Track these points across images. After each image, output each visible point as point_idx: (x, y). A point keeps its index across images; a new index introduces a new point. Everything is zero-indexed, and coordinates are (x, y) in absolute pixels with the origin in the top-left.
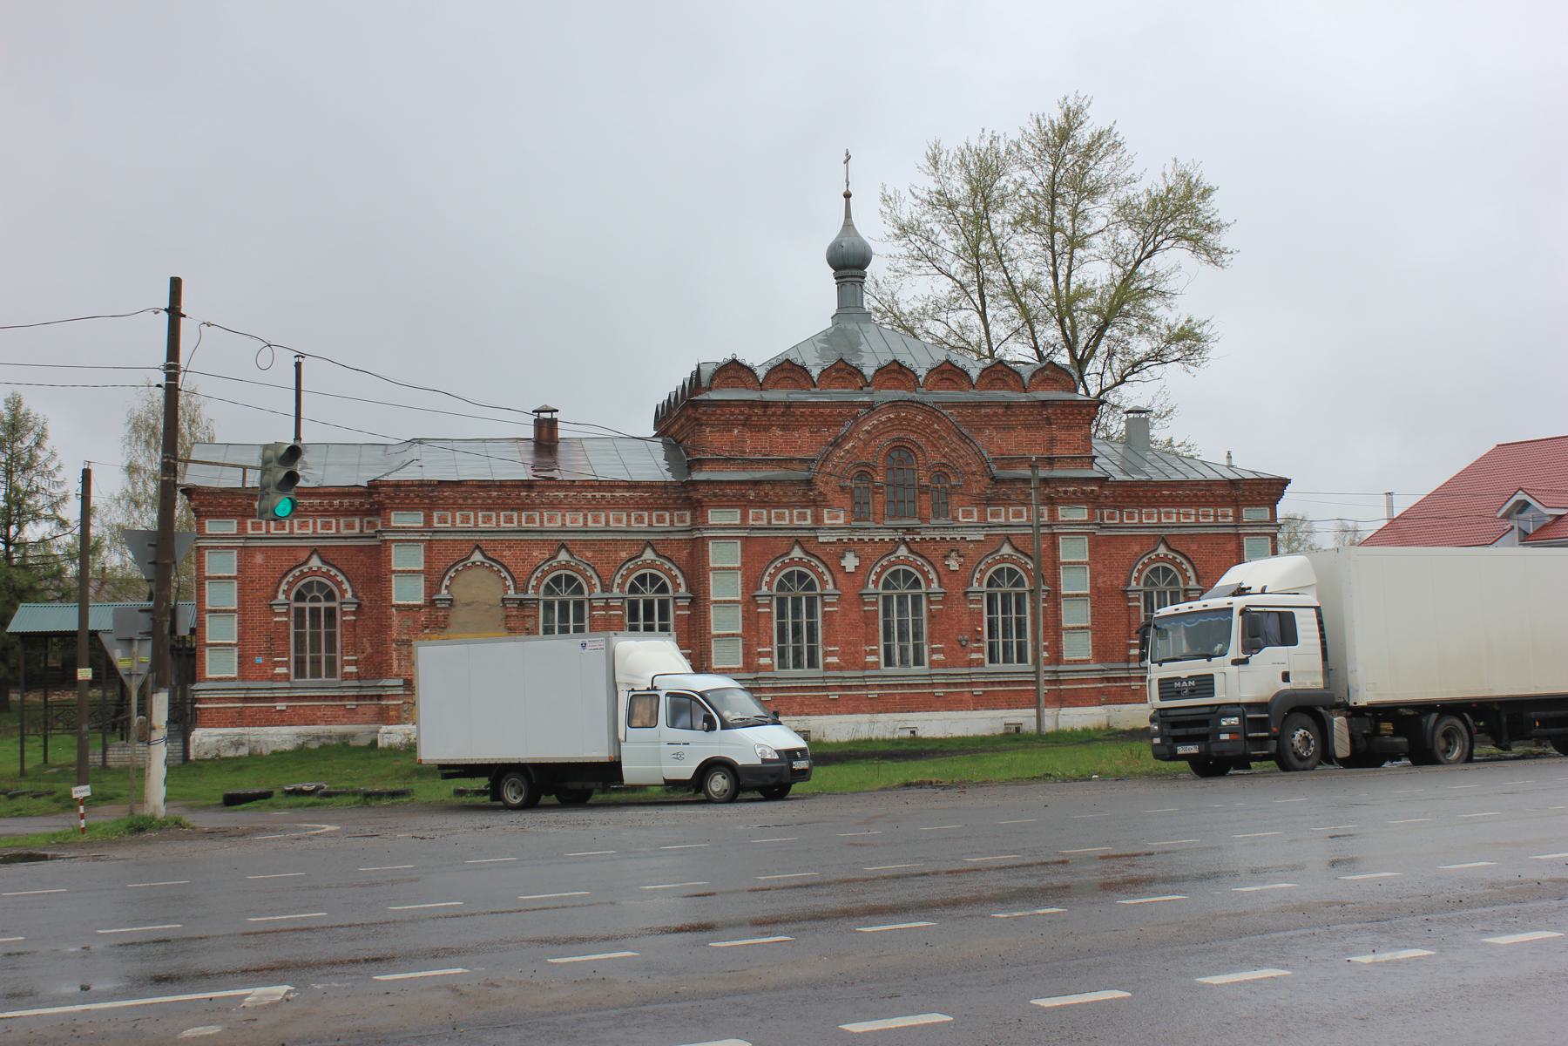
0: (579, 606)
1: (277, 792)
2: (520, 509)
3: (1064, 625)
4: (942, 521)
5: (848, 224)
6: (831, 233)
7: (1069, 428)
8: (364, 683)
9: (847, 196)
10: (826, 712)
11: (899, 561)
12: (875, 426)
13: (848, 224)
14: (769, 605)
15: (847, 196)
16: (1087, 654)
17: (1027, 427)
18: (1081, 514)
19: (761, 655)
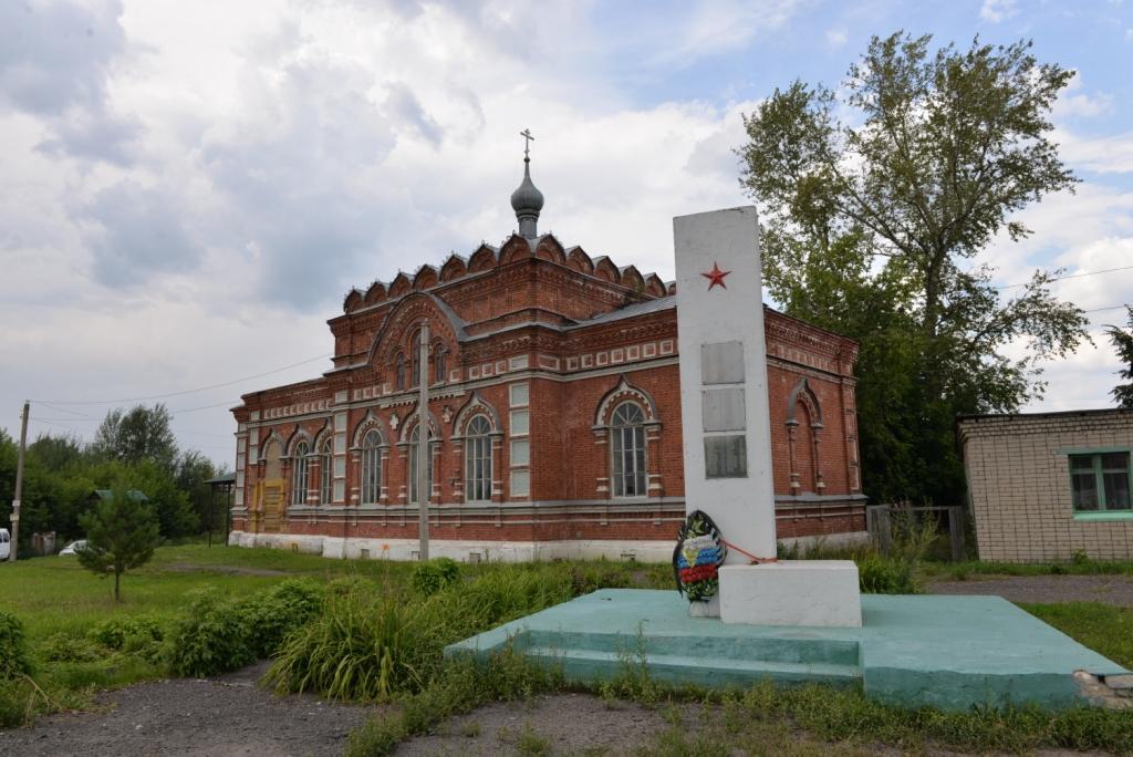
0: (640, 431)
1: (909, 566)
2: (290, 404)
3: (512, 465)
4: (442, 383)
5: (527, 180)
6: (516, 184)
7: (518, 288)
8: (666, 500)
9: (527, 160)
10: (649, 537)
11: (623, 397)
12: (404, 317)
13: (527, 180)
14: (606, 438)
15: (527, 160)
16: (526, 493)
17: (495, 294)
18: (522, 362)
19: (601, 483)
